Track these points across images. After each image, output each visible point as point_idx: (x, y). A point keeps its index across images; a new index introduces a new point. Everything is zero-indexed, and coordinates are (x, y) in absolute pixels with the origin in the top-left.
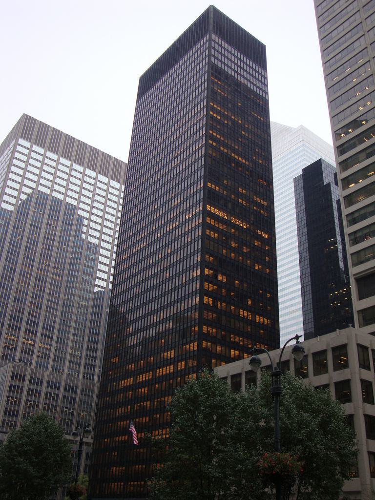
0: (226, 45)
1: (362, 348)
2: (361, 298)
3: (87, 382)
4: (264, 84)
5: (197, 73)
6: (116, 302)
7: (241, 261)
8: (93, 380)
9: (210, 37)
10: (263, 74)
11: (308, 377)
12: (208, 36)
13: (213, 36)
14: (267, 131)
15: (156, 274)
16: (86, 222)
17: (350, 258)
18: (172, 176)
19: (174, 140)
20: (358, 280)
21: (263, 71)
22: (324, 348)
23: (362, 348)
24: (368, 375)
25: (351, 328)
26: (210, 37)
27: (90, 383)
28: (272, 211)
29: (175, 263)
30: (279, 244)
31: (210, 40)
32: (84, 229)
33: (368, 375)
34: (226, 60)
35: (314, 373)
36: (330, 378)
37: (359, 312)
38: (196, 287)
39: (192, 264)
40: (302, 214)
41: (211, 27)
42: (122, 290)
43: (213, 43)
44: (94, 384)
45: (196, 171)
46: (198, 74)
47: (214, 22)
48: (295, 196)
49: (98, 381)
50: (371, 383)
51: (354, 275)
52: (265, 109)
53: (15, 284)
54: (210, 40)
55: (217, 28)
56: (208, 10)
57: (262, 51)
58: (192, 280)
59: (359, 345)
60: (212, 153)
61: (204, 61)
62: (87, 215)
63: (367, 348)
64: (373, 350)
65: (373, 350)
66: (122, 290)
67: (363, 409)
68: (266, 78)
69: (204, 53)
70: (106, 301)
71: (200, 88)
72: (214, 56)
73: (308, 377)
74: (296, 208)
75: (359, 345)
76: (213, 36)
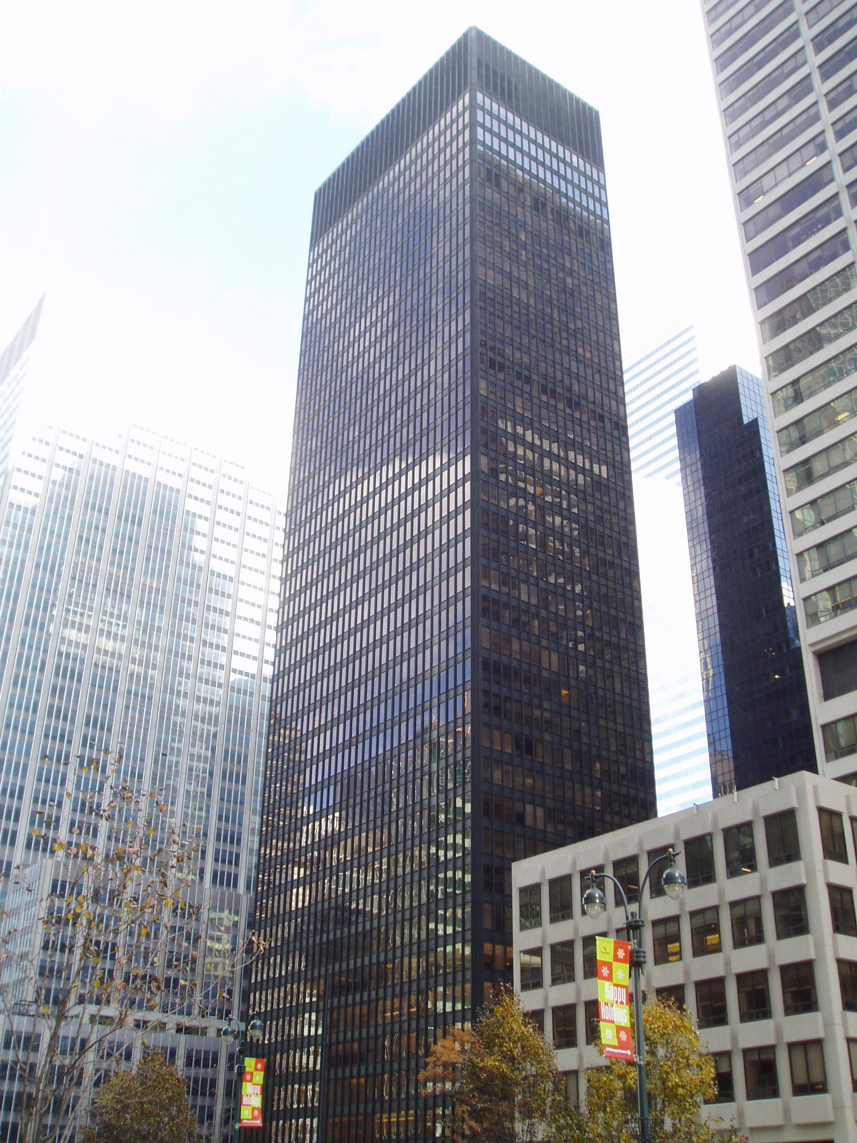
0: (510, 116)
1: (828, 817)
2: (828, 694)
3: (223, 894)
4: (599, 200)
5: (445, 165)
6: (286, 710)
7: (561, 613)
8: (235, 886)
9: (473, 99)
10: (596, 177)
11: (715, 881)
12: (467, 97)
13: (479, 96)
14: (616, 393)
15: (371, 647)
16: (201, 526)
17: (783, 481)
18: (399, 399)
19: (404, 376)
20: (822, 657)
21: (595, 171)
22: (747, 817)
23: (828, 817)
24: (840, 874)
25: (806, 774)
26: (473, 99)
27: (231, 895)
28: (646, 735)
29: (414, 622)
30: (658, 721)
31: (473, 106)
32: (199, 542)
33: (840, 874)
34: (511, 133)
35: (734, 943)
36: (763, 883)
37: (824, 727)
38: (464, 709)
39: (452, 564)
40: (711, 618)
41: (473, 76)
42: (298, 659)
43: (480, 114)
44: (238, 897)
45: (454, 339)
46: (448, 168)
47: (479, 62)
48: (710, 744)
49: (248, 888)
50: (849, 891)
51: (812, 645)
52: (627, 545)
53: (31, 779)
54: (473, 106)
55: (488, 79)
56: (465, 36)
57: (592, 127)
58: (453, 570)
59: (821, 810)
60: (500, 588)
61: (461, 138)
62: (205, 510)
63: (839, 815)
64: (853, 819)
65: (853, 819)
66: (298, 659)
67: (826, 872)
68: (603, 187)
69: (461, 120)
70: (259, 725)
71: (454, 162)
72: (483, 126)
73: (715, 881)
74: (708, 736)
75: (821, 810)
76: (479, 96)
